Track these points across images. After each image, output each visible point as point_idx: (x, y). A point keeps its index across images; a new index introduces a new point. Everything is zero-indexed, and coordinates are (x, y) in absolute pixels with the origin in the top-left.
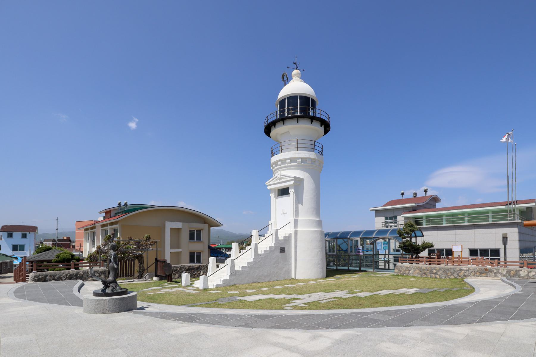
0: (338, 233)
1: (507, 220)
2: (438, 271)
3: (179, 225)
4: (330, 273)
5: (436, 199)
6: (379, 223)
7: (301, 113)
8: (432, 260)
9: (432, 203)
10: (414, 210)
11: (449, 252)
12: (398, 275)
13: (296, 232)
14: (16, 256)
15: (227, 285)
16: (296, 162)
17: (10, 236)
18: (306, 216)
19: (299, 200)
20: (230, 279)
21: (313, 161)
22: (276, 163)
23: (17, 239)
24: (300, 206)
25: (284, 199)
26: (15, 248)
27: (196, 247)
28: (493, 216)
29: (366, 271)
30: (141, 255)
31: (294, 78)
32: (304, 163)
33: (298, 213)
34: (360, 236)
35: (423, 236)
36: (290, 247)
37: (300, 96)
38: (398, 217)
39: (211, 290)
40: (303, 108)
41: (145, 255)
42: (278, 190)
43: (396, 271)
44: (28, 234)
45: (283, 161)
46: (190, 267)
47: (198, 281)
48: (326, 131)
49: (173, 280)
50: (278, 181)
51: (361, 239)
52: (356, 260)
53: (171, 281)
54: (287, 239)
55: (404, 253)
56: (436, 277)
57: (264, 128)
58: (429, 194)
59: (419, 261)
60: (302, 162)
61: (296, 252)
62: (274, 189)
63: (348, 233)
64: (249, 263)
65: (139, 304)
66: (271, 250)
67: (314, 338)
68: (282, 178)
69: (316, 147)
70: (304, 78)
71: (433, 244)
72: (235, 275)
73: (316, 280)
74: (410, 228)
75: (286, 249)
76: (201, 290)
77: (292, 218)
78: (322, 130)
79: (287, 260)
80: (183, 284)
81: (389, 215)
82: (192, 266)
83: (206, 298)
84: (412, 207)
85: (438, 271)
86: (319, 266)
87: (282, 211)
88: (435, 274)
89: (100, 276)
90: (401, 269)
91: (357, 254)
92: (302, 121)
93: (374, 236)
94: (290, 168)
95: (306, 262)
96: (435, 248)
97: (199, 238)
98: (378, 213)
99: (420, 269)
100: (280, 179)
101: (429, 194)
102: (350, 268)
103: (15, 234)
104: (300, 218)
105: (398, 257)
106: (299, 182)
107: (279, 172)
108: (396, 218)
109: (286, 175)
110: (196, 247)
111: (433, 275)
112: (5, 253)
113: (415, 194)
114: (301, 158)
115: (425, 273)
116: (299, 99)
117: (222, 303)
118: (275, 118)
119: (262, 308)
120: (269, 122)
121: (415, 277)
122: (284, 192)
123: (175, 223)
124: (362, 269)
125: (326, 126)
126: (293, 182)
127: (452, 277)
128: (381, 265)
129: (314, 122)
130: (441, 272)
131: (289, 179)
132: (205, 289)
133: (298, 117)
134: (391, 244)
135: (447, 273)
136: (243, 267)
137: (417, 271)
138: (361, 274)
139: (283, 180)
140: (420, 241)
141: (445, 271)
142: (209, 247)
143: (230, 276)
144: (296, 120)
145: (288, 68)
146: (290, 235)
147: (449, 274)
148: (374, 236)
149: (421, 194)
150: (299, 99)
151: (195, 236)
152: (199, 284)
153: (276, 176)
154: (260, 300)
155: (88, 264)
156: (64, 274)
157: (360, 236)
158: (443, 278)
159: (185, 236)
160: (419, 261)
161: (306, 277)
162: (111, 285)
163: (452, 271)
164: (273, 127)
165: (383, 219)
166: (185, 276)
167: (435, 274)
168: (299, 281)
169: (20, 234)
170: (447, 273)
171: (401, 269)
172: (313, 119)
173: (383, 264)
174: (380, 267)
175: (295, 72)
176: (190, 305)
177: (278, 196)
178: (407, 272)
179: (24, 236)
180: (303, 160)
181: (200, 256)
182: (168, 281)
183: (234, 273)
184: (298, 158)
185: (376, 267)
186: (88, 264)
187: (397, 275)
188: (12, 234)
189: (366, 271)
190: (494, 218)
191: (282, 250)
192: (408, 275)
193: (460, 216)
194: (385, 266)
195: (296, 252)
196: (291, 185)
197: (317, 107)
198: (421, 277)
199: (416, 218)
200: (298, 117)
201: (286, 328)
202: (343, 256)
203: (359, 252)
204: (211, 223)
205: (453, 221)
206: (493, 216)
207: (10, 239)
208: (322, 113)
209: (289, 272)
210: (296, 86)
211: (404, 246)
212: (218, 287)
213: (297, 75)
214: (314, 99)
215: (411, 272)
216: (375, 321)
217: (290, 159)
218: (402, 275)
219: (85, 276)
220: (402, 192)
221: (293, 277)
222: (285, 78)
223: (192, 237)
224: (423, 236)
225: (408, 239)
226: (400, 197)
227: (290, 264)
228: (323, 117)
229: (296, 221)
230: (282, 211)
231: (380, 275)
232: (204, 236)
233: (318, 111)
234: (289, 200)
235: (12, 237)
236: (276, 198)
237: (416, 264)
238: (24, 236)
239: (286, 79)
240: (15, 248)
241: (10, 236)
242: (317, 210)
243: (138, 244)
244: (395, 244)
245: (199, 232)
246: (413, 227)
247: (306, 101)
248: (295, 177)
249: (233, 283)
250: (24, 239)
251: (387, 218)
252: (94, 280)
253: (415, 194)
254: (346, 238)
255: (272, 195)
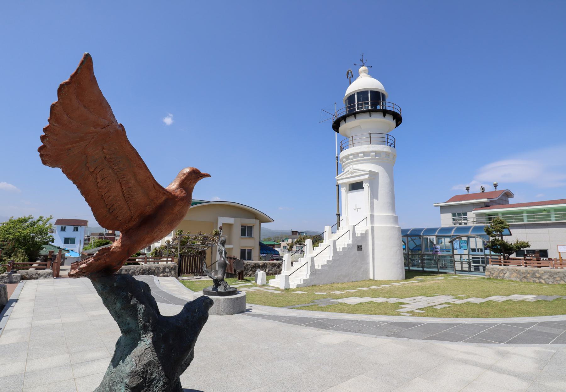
0: (408, 230)
1: (512, 222)
2: (543, 274)
3: (231, 220)
4: (409, 274)
5: (508, 194)
6: (447, 220)
7: (372, 107)
8: (527, 261)
9: (504, 198)
10: (487, 205)
11: (544, 253)
12: (490, 279)
13: (373, 228)
14: (68, 249)
15: (308, 285)
16: (369, 155)
17: (63, 229)
18: (382, 212)
19: (374, 195)
20: (310, 279)
21: (387, 154)
22: (347, 157)
23: (69, 232)
24: (375, 201)
25: (357, 194)
26: (67, 241)
27: (248, 243)
28: (528, 216)
29: (445, 273)
30: (204, 251)
31: (361, 75)
32: (377, 157)
33: (373, 208)
34: (436, 234)
35: (511, 235)
36: (367, 245)
37: (371, 91)
38: (468, 213)
39: (294, 290)
40: (373, 102)
41: (208, 252)
42: (349, 184)
43: (487, 273)
44: (79, 228)
45: (356, 155)
46: (255, 264)
47: (273, 280)
48: (397, 125)
49: (244, 278)
50: (350, 175)
51: (437, 236)
52: (429, 260)
53: (243, 279)
54: (364, 236)
55: (492, 253)
56: (540, 282)
57: (332, 123)
58: (498, 189)
59: (509, 262)
60: (376, 156)
61: (373, 250)
62: (345, 183)
63: (420, 230)
64: (328, 261)
65: (248, 306)
66: (349, 247)
67: (503, 355)
68: (355, 172)
69: (389, 141)
70: (372, 73)
71: (529, 244)
72: (315, 274)
73: (397, 281)
74: (500, 225)
75: (363, 247)
76: (282, 290)
77: (368, 214)
78: (394, 123)
79: (364, 259)
80: (259, 282)
81: (458, 212)
82: (258, 264)
83: (285, 298)
84: (484, 203)
85: (543, 274)
86: (399, 265)
87: (355, 206)
88: (539, 278)
89: (170, 272)
90: (493, 272)
91: (435, 253)
92: (373, 115)
93: (452, 233)
94: (363, 162)
95: (385, 263)
96: (532, 248)
97: (250, 234)
98: (444, 209)
99: (518, 272)
100: (352, 173)
101: (498, 189)
102: (425, 269)
103: (68, 227)
104: (376, 214)
105: (479, 258)
106: (373, 176)
107: (351, 166)
108: (465, 214)
109: (359, 169)
110: (248, 243)
111: (537, 280)
112: (58, 246)
113: (483, 189)
114: (375, 152)
115: (525, 277)
116: (369, 94)
117: (323, 306)
118: (344, 114)
119: (365, 312)
120: (339, 116)
121: (512, 281)
122: (356, 186)
123: (227, 218)
124: (440, 270)
125: (398, 119)
126: (368, 176)
127: (562, 282)
128: (458, 266)
129: (387, 116)
130: (547, 276)
131: (363, 173)
132: (287, 289)
133: (369, 111)
134: (471, 243)
135: (554, 278)
136: (322, 266)
137: (515, 275)
138: (441, 277)
139: (355, 174)
140: (509, 240)
141: (551, 275)
142: (261, 244)
143: (311, 275)
144: (368, 114)
145: (355, 65)
146: (367, 231)
147: (558, 279)
148: (452, 233)
149: (489, 189)
150: (369, 94)
151: (246, 231)
152: (278, 282)
153: (346, 170)
154: (361, 303)
155: (153, 260)
156: (138, 269)
157: (436, 234)
158: (551, 283)
159: (237, 231)
160: (509, 262)
161: (386, 279)
162: (222, 283)
163: (561, 275)
164: (343, 121)
165: (449, 216)
166: (261, 274)
167: (539, 278)
168: (379, 283)
169: (72, 227)
170: (554, 278)
171: (493, 272)
172: (385, 112)
173: (460, 265)
174: (457, 269)
175: (362, 68)
176: (293, 307)
177: (350, 190)
178: (501, 275)
179: (76, 229)
180: (377, 153)
181: (251, 252)
182: (239, 279)
183: (314, 272)
184: (372, 152)
185: (453, 268)
186: (153, 260)
187: (488, 279)
188: (65, 228)
189: (445, 273)
190: (557, 217)
191: (360, 248)
192: (503, 279)
193: (545, 213)
194: (462, 267)
195: (373, 250)
196: (366, 179)
197: (387, 101)
198: (521, 281)
199: (489, 215)
200: (369, 111)
201: (450, 341)
202: (420, 256)
203: (437, 251)
204: (262, 219)
205: (534, 218)
206: (528, 216)
207: (63, 232)
208: (395, 106)
209: (367, 271)
210: (364, 81)
211: (493, 246)
212: (299, 287)
213: (364, 71)
214: (385, 93)
215: (506, 275)
216: (552, 336)
217: (362, 151)
218: (496, 278)
219: (156, 272)
220: (467, 186)
221: (372, 278)
222: (350, 75)
223: (243, 233)
224: (511, 235)
225: (497, 237)
226: (466, 192)
227: (368, 263)
228: (396, 111)
229: (372, 217)
230: (355, 206)
231: (467, 278)
232: (255, 231)
233: (387, 104)
234: (363, 195)
235: (64, 230)
236: (347, 193)
237: (504, 265)
238: (76, 229)
239: (351, 76)
240: (67, 241)
241: (63, 229)
242: (393, 206)
243: (205, 239)
244: (477, 243)
245: (250, 228)
246: (498, 226)
247: (377, 96)
248: (370, 171)
249: (313, 283)
250: (76, 233)
251: (454, 215)
252: (165, 276)
253: (483, 189)
254: (419, 236)
255: (343, 190)
